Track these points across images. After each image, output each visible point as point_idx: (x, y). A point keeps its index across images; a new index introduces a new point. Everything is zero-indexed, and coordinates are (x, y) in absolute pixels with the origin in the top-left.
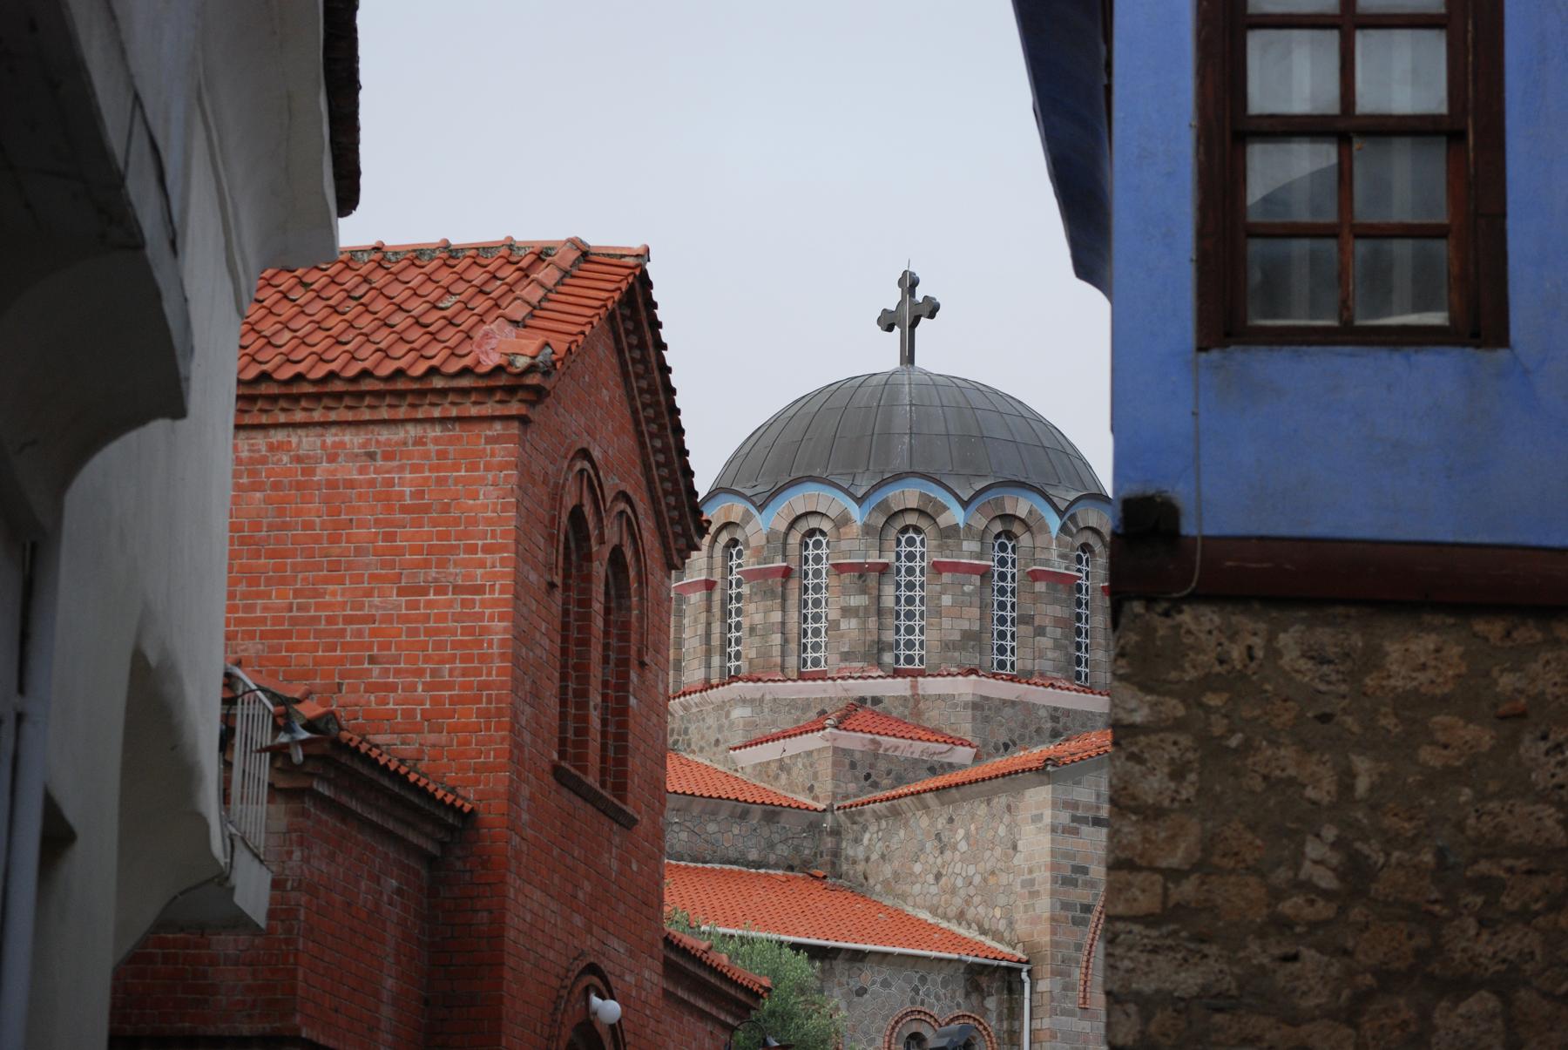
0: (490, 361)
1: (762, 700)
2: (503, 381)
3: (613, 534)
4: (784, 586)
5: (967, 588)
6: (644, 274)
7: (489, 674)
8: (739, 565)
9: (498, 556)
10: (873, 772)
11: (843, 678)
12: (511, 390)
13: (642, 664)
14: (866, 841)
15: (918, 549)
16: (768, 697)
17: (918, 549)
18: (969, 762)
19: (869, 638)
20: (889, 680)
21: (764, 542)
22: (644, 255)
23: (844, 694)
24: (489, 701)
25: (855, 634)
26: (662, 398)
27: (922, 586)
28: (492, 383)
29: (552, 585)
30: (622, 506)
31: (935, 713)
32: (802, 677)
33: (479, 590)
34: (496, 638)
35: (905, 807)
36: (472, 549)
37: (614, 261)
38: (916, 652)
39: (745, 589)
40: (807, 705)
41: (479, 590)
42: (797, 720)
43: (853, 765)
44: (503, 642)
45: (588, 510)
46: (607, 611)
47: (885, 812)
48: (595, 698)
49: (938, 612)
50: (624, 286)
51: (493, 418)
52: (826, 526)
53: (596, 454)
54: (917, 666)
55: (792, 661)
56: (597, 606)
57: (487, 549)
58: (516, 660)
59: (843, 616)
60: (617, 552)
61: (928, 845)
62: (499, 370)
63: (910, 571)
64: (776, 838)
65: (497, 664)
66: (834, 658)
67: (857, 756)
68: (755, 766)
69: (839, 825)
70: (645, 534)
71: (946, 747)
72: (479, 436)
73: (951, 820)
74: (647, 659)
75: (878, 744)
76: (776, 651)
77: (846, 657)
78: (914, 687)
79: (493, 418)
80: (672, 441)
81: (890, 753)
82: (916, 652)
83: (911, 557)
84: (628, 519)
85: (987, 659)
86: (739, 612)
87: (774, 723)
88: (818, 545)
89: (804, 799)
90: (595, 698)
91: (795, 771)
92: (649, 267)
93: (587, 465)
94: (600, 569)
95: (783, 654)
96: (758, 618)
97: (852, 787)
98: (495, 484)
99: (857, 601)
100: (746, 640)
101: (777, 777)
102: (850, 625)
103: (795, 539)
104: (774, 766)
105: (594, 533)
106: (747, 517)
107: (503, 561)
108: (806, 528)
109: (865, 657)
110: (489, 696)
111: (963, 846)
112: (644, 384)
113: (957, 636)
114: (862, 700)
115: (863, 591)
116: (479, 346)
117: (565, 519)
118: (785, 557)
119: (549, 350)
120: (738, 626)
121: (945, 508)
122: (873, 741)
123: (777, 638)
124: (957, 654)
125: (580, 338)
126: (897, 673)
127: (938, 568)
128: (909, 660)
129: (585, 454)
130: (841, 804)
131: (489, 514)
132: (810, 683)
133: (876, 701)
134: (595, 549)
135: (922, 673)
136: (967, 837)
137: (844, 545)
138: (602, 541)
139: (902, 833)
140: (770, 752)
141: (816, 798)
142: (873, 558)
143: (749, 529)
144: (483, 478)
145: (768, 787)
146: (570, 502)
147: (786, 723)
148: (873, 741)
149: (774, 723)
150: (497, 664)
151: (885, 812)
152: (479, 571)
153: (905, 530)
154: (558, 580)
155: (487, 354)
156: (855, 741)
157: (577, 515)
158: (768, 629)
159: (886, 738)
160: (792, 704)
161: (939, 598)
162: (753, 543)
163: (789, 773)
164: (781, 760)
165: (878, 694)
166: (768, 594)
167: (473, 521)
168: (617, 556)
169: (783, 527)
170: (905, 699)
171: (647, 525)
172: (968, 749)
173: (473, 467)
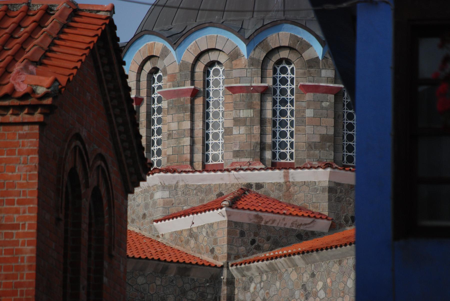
0: (22, 89)
1: (176, 187)
2: (30, 101)
3: (93, 182)
4: (192, 103)
5: (324, 104)
6: (112, 21)
7: (22, 278)
8: (160, 87)
9: (27, 206)
10: (257, 238)
11: (235, 170)
12: (33, 108)
13: (111, 256)
14: (252, 289)
15: (289, 76)
16: (181, 184)
17: (289, 76)
18: (326, 230)
19: (253, 141)
20: (270, 171)
21: (177, 70)
22: (112, 10)
23: (235, 182)
24: (22, 294)
25: (243, 138)
26: (122, 93)
27: (292, 102)
28: (23, 103)
29: (58, 219)
30: (99, 162)
31: (301, 195)
32: (205, 168)
33: (16, 227)
34: (26, 256)
35: (280, 265)
36: (11, 202)
37: (93, 14)
38: (287, 151)
39: (164, 104)
40: (208, 189)
41: (16, 227)
42: (202, 200)
43: (242, 234)
44: (30, 258)
45: (79, 169)
46: (90, 225)
47: (266, 268)
48: (84, 282)
49: (302, 121)
50: (99, 32)
51: (23, 124)
52: (223, 58)
53: (84, 134)
54: (288, 160)
55: (198, 157)
56: (85, 226)
57: (20, 202)
58: (38, 269)
59: (235, 125)
60: (96, 191)
61: (297, 293)
62: (26, 96)
63: (284, 92)
64: (187, 287)
65: (26, 272)
66: (229, 155)
67: (246, 227)
68: (171, 234)
69: (233, 278)
70: (112, 176)
71: (310, 220)
72: (14, 134)
73: (313, 275)
74: (114, 253)
75: (261, 218)
76: (187, 150)
77: (237, 154)
78: (286, 176)
79: (23, 124)
80: (129, 119)
81: (269, 224)
82: (287, 151)
83: (284, 81)
84: (103, 169)
85: (340, 155)
86: (160, 121)
87: (185, 202)
88: (217, 72)
89: (208, 258)
90: (84, 282)
91: (200, 238)
92: (114, 17)
93: (78, 143)
94: (86, 203)
95: (192, 152)
96: (174, 126)
97: (242, 249)
98: (25, 163)
99: (245, 113)
100: (165, 142)
101: (187, 242)
102: (240, 132)
103: (200, 68)
104: (185, 234)
105: (82, 181)
106: (165, 53)
107: (30, 210)
108: (206, 63)
109: (250, 154)
110: (22, 292)
111: (322, 294)
112: (120, 120)
113: (317, 139)
114: (249, 185)
115: (250, 106)
116: (14, 80)
117: (66, 178)
118: (193, 83)
119: (57, 84)
120: (159, 131)
121: (309, 46)
122: (257, 216)
123: (187, 141)
124: (317, 152)
125: (75, 71)
126: (274, 166)
127: (306, 89)
128: (283, 156)
129: (78, 136)
130: (234, 262)
131: (22, 181)
132: (212, 173)
133: (259, 186)
134: (83, 191)
135: (291, 166)
136: (325, 288)
137: (235, 73)
138: (87, 186)
139: (278, 284)
140: (182, 224)
141: (216, 258)
142: (257, 83)
143: (166, 61)
144: (18, 160)
145: (181, 249)
146: (68, 167)
147: (195, 203)
148: (257, 216)
149: (185, 202)
150: (26, 272)
151: (266, 268)
152: (16, 216)
153: (279, 62)
154: (62, 216)
155: (19, 84)
156: (244, 217)
157: (73, 174)
158: (180, 134)
159: (266, 214)
160: (199, 189)
161: (304, 112)
162: (169, 71)
163: (196, 239)
164: (191, 230)
165: (261, 181)
166: (180, 108)
167: (13, 186)
168: (96, 192)
169: (191, 60)
170: (280, 185)
171: (114, 169)
172: (325, 221)
173: (12, 152)
